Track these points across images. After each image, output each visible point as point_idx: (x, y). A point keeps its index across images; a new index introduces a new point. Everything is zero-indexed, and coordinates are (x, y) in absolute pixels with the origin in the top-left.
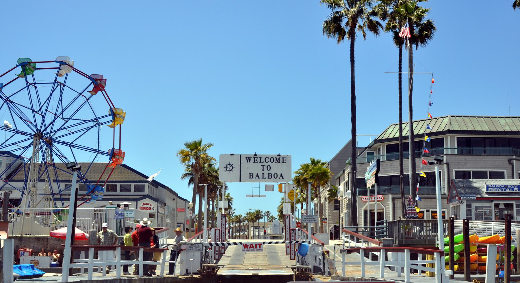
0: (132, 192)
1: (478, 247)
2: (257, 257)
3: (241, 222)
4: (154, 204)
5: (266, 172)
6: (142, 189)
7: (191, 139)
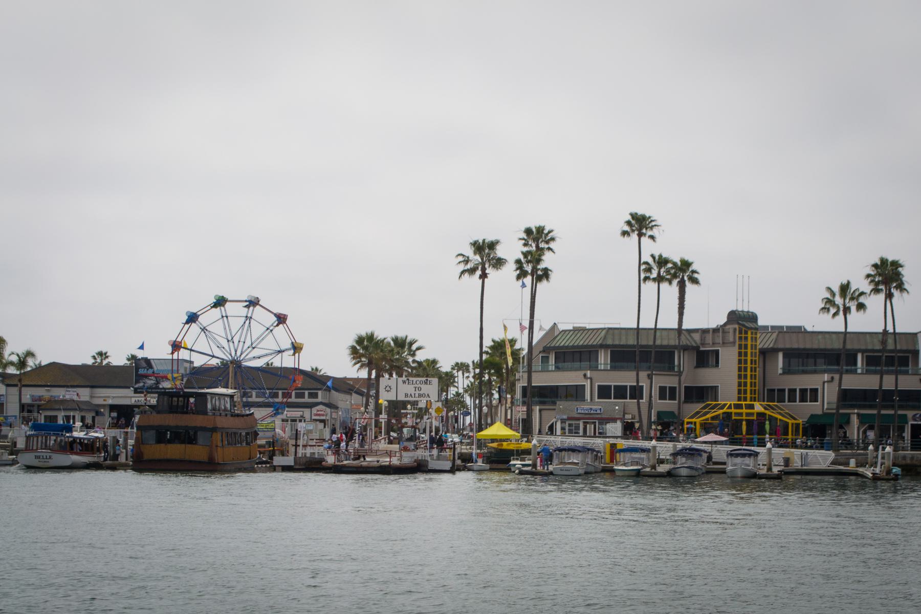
5: (417, 392)
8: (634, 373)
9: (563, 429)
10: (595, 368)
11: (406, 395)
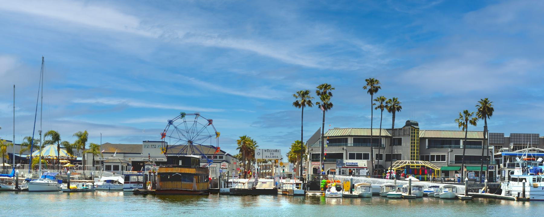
0: (218, 159)
1: (283, 192)
2: (462, 127)
3: (266, 162)
4: (227, 164)
5: (272, 156)
6: (222, 158)
7: (242, 136)
8: (370, 148)
9: (340, 172)
10: (346, 145)
11: (266, 157)
